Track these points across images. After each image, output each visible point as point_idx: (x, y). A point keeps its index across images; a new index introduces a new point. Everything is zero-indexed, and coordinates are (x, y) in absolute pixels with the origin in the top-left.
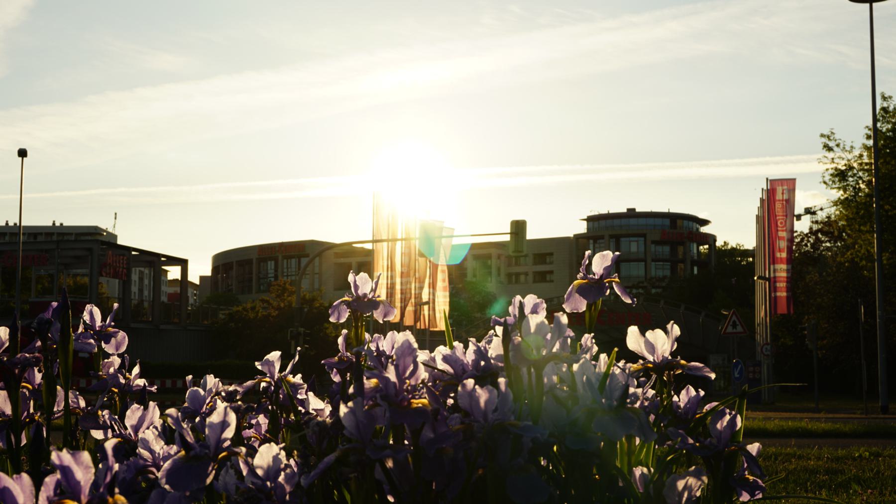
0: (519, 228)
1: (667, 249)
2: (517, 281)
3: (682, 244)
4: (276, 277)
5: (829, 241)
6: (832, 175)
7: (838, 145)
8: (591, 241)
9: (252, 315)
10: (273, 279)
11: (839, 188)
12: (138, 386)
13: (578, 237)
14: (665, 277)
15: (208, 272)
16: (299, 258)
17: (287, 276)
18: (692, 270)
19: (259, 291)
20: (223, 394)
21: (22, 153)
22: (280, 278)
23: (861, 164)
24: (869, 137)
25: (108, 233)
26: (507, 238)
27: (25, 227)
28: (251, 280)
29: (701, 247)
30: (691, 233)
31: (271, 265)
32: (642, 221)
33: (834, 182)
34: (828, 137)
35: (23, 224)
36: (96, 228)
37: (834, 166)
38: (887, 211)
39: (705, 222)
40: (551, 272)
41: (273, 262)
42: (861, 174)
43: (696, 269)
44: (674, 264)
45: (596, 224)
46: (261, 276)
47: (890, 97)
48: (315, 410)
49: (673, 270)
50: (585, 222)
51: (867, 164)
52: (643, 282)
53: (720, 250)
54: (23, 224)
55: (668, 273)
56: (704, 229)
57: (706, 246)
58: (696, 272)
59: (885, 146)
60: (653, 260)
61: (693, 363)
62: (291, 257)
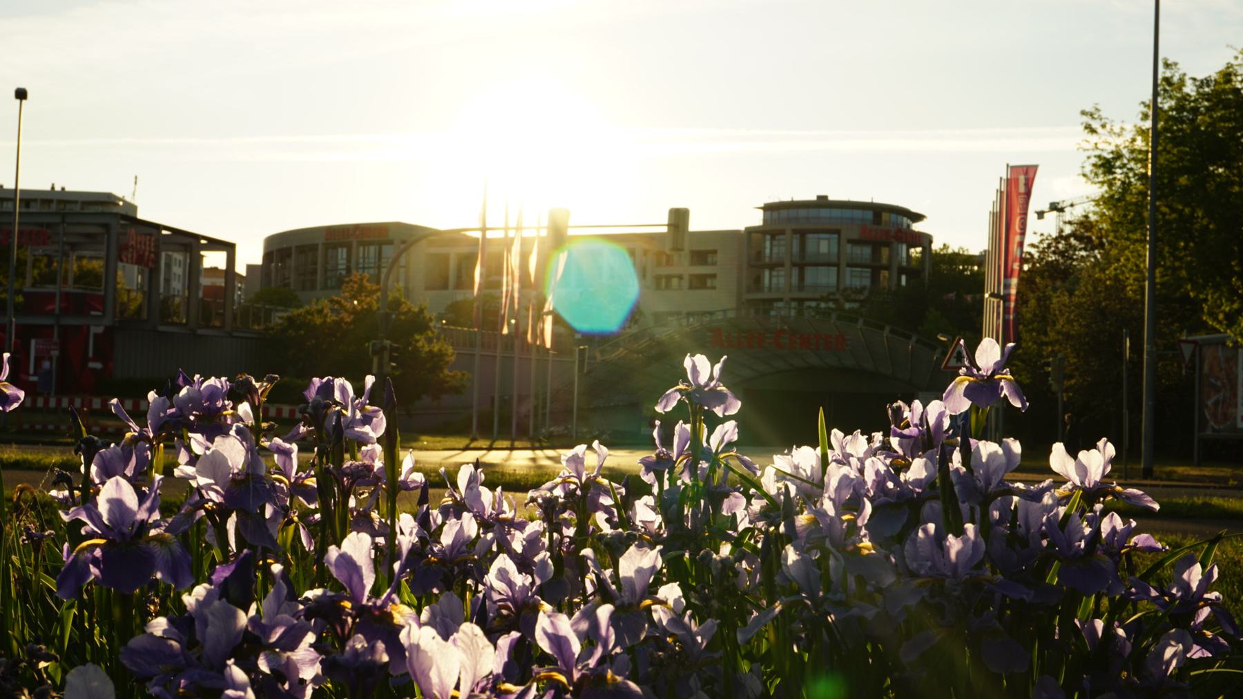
0: (679, 217)
1: (867, 251)
2: (668, 286)
3: (888, 244)
4: (349, 270)
5: (1085, 249)
6: (1094, 165)
7: (1103, 126)
8: (768, 237)
9: (318, 320)
10: (344, 272)
11: (1103, 183)
12: (414, 481)
13: (750, 231)
14: (863, 289)
15: (258, 261)
16: (380, 244)
17: (364, 268)
18: (899, 280)
19: (325, 287)
20: (540, 501)
21: (21, 94)
22: (354, 272)
23: (1132, 151)
24: (1145, 117)
25: (125, 202)
26: (665, 230)
27: (22, 191)
28: (314, 272)
29: (912, 250)
30: (900, 230)
31: (342, 253)
32: (836, 213)
33: (1096, 175)
34: (1091, 115)
35: (20, 187)
36: (109, 195)
37: (1098, 152)
38: (1164, 214)
39: (918, 217)
40: (714, 276)
41: (345, 250)
42: (1132, 165)
43: (904, 278)
44: (876, 270)
45: (775, 214)
46: (329, 267)
47: (1176, 64)
48: (643, 522)
49: (875, 278)
50: (761, 212)
51: (1140, 152)
52: (834, 294)
53: (937, 254)
54: (20, 187)
55: (867, 282)
56: (917, 227)
57: (919, 249)
58: (904, 282)
59: (1165, 129)
60: (849, 265)
61: (1130, 490)
62: (370, 244)
